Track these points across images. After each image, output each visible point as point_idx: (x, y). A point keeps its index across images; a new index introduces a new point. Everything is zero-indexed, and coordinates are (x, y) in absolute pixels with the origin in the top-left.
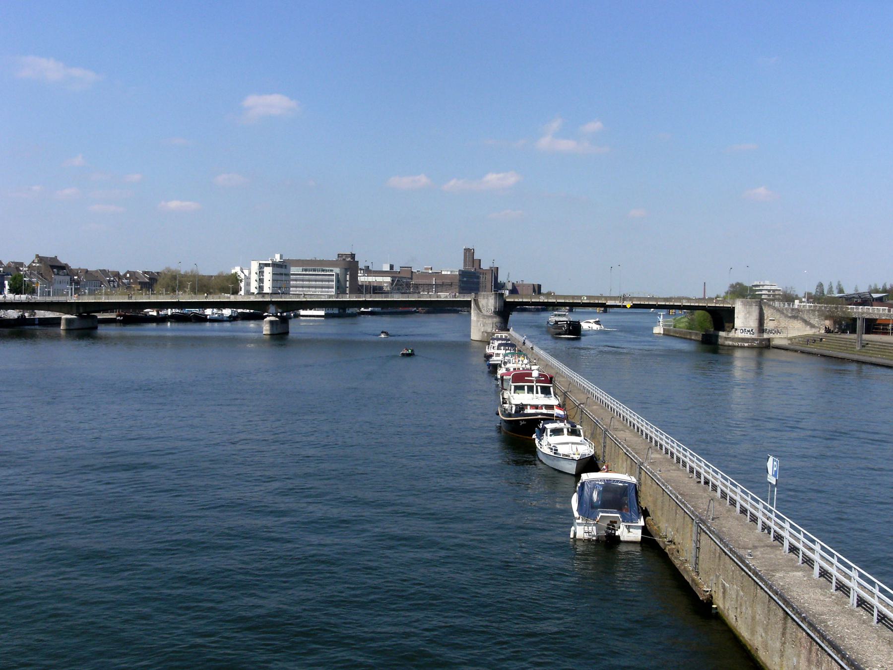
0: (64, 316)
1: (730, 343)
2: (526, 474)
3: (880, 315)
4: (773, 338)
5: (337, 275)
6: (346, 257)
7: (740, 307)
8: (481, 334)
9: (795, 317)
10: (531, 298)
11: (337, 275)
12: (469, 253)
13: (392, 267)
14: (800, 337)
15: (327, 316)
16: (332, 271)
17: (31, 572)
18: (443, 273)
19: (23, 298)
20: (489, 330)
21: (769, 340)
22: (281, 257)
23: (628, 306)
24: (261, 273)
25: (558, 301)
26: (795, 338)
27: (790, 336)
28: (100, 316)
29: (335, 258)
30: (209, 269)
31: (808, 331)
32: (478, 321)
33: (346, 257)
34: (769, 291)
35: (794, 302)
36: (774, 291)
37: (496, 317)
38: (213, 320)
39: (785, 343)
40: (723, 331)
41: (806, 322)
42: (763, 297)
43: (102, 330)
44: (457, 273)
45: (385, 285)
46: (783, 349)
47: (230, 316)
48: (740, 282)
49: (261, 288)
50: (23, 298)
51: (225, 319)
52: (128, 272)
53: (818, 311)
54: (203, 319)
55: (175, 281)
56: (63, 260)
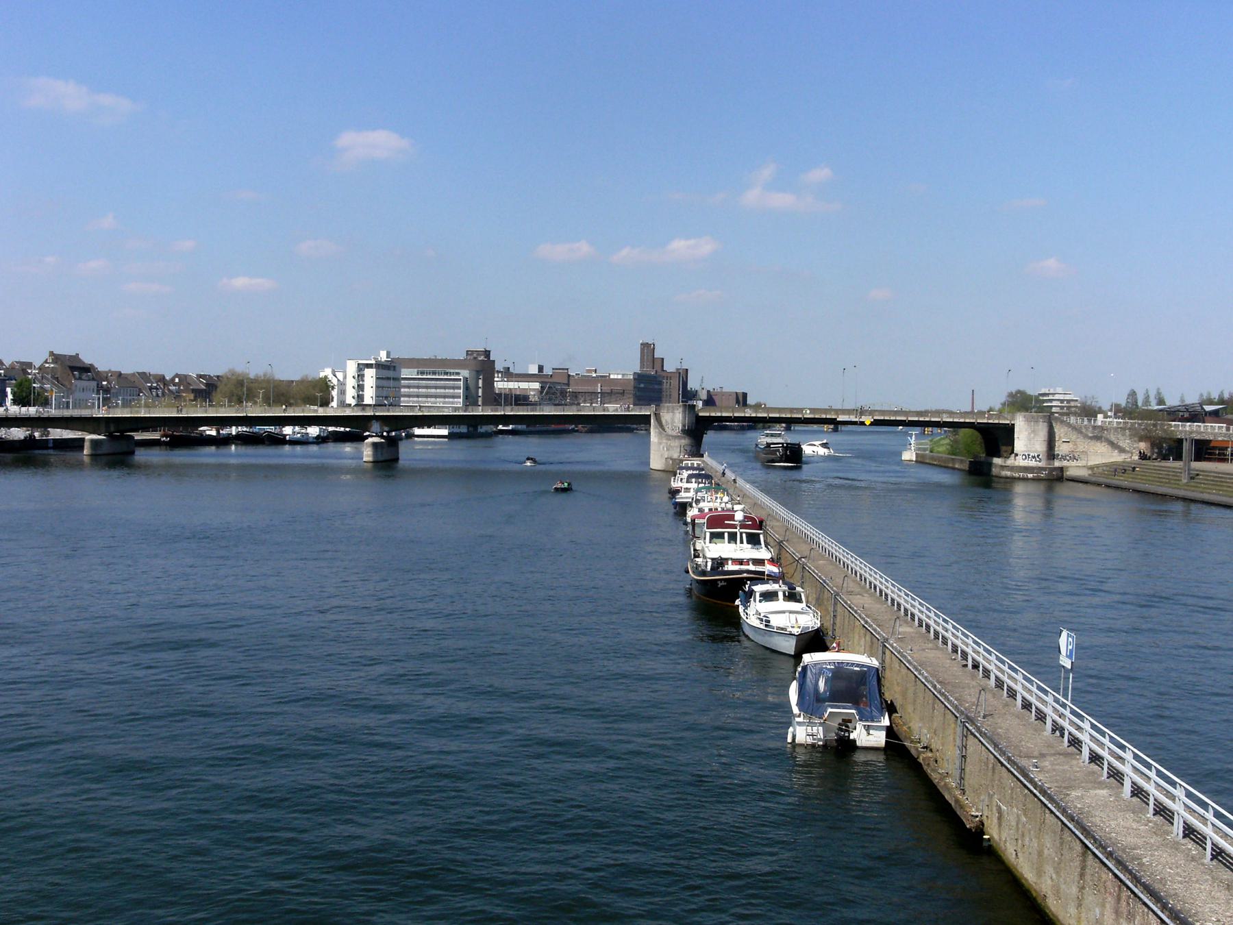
0: (89, 437)
1: (1008, 473)
2: (726, 654)
3: (1215, 435)
4: (1067, 467)
5: (466, 379)
6: (478, 355)
7: (1022, 423)
8: (664, 461)
9: (1097, 438)
10: (733, 412)
11: (466, 379)
12: (647, 349)
13: (541, 368)
14: (1105, 465)
15: (451, 436)
16: (458, 374)
17: (43, 790)
18: (612, 377)
19: (32, 411)
20: (675, 456)
21: (1061, 469)
22: (388, 355)
23: (868, 423)
24: (360, 377)
25: (770, 415)
26: (1097, 466)
27: (1090, 463)
28: (139, 436)
29: (462, 356)
30: (288, 371)
31: (1116, 457)
32: (660, 443)
33: (478, 355)
34: (1062, 401)
35: (1096, 417)
36: (1069, 401)
37: (685, 438)
38: (294, 442)
39: (1083, 473)
40: (999, 457)
41: (1113, 445)
42: (1054, 410)
43: (141, 455)
44: (632, 377)
45: (532, 393)
46: (1081, 482)
47: (318, 437)
48: (1021, 389)
49: (360, 398)
50: (32, 411)
51: (311, 440)
52: (177, 376)
53: (1130, 429)
54: (280, 441)
55: (242, 389)
56: (87, 359)
